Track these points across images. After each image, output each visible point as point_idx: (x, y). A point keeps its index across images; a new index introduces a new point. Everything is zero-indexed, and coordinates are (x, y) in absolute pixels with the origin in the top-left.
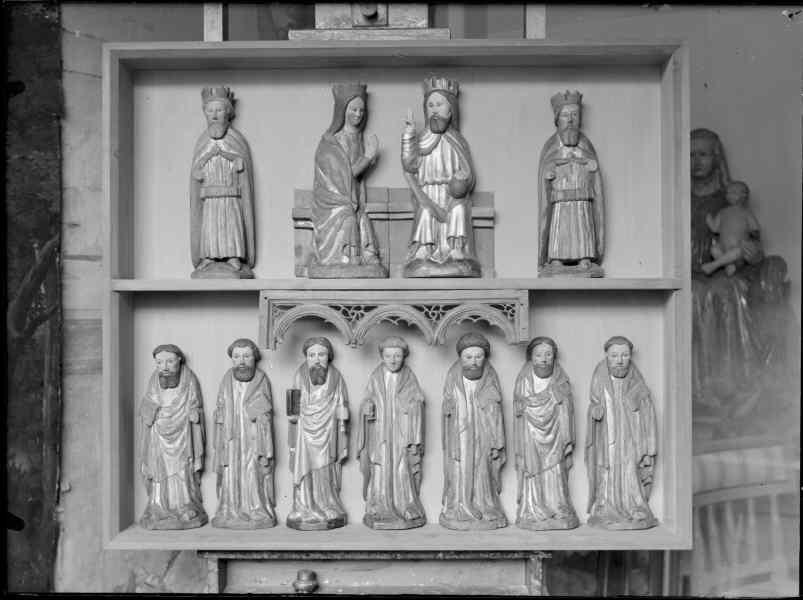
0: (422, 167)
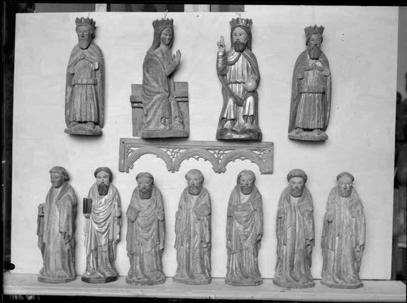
0: (229, 72)
